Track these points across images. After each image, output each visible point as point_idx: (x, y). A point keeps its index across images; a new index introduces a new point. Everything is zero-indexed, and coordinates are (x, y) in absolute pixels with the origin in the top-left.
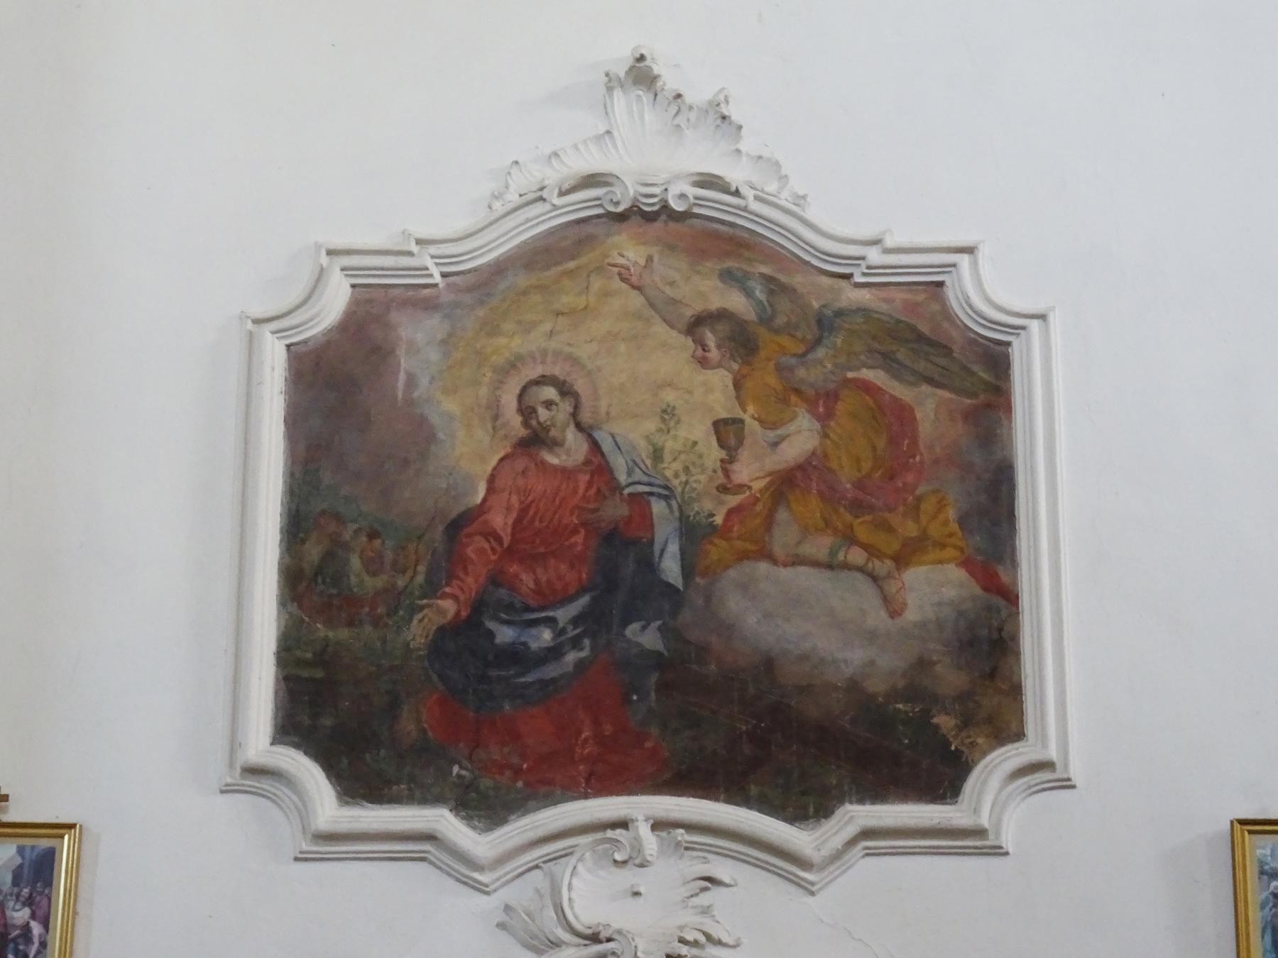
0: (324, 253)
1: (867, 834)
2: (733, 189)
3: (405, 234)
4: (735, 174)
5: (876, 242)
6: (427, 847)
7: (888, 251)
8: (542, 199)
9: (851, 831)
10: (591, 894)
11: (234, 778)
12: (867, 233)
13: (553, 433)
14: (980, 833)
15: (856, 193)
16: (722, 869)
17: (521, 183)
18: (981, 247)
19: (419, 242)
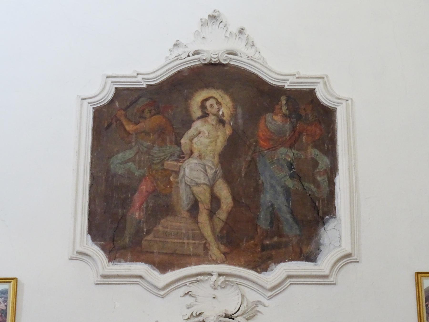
7: (298, 78)
12: (292, 72)
19: (138, 74)
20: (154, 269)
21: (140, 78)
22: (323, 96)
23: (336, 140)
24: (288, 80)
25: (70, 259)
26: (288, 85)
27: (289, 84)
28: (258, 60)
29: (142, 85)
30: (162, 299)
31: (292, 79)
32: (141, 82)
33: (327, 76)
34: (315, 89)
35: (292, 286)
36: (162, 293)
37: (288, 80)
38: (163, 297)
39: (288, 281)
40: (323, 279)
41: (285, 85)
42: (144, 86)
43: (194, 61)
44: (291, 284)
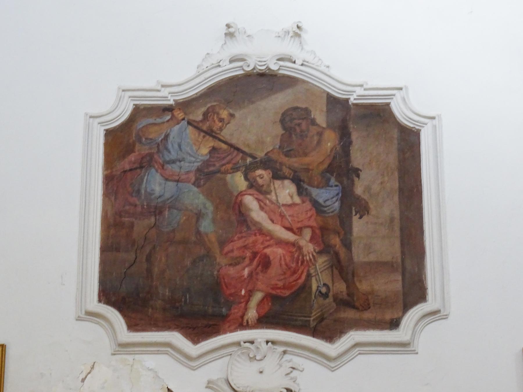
0: (121, 91)
1: (357, 345)
2: (294, 60)
3: (158, 82)
4: (299, 56)
5: (361, 86)
6: (169, 349)
7: (365, 90)
8: (219, 66)
9: (352, 343)
10: (243, 373)
11: (83, 315)
12: (359, 82)
13: (265, 188)
14: (414, 351)
15: (348, 63)
16: (297, 361)
17: (214, 61)
18: (228, 63)
19: (163, 86)
20: (365, 331)
21: (165, 92)
22: (401, 112)
23: (101, 226)
24: (355, 92)
25: (77, 320)
26: (355, 99)
27: (356, 97)
28: (317, 67)
29: (169, 100)
30: (331, 372)
31: (360, 91)
32: (167, 97)
33: (406, 88)
34: (388, 104)
35: (359, 356)
36: (332, 365)
37: (355, 92)
38: (193, 369)
39: (357, 349)
40: (403, 346)
41: (349, 99)
42: (172, 102)
43: (235, 70)
44: (360, 354)
